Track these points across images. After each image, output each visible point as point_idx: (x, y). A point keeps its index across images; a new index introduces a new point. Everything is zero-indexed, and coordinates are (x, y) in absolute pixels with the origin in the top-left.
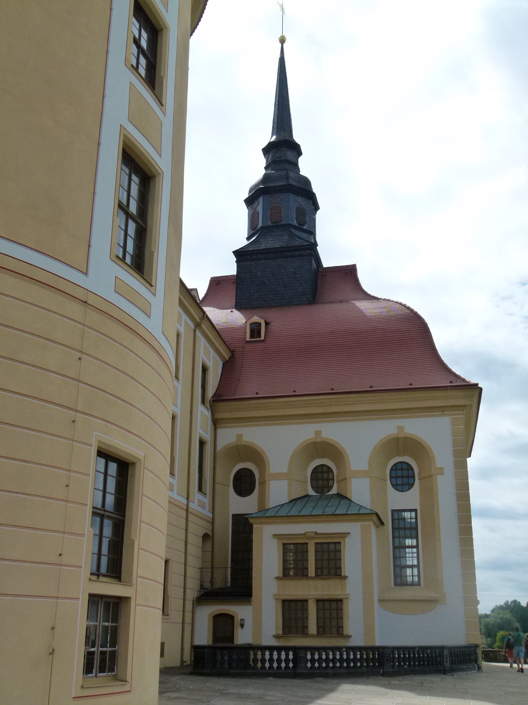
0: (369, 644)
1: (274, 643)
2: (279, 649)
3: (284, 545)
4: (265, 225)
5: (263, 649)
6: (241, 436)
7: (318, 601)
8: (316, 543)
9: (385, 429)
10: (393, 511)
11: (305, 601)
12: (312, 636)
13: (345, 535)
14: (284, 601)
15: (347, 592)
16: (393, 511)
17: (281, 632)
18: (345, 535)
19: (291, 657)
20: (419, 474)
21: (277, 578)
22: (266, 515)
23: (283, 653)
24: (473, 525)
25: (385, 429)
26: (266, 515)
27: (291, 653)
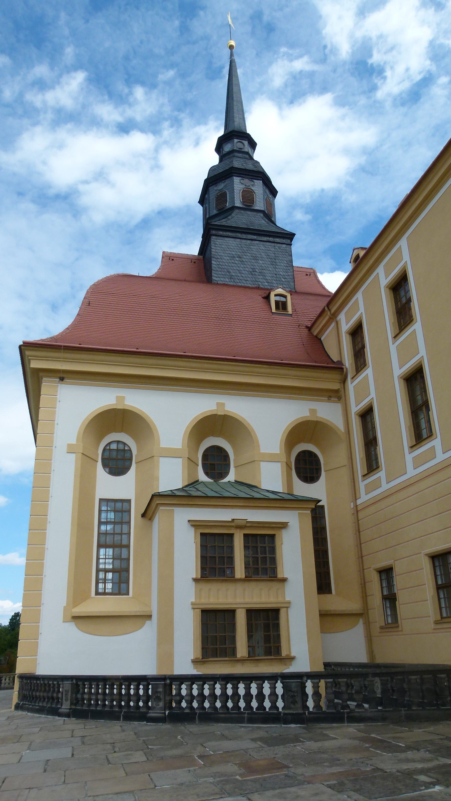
0: (166, 672)
1: (191, 670)
2: (202, 679)
3: (202, 534)
4: (227, 181)
5: (181, 679)
6: (123, 398)
7: (250, 613)
8: (245, 535)
9: (203, 404)
10: (101, 500)
11: (232, 612)
12: (242, 661)
13: (284, 526)
14: (204, 612)
15: (287, 599)
16: (101, 500)
17: (199, 656)
18: (284, 526)
19: (279, 690)
20: (235, 460)
21: (195, 580)
22: (186, 496)
23: (254, 686)
24: (175, 522)
25: (203, 404)
26: (186, 496)
27: (279, 685)
